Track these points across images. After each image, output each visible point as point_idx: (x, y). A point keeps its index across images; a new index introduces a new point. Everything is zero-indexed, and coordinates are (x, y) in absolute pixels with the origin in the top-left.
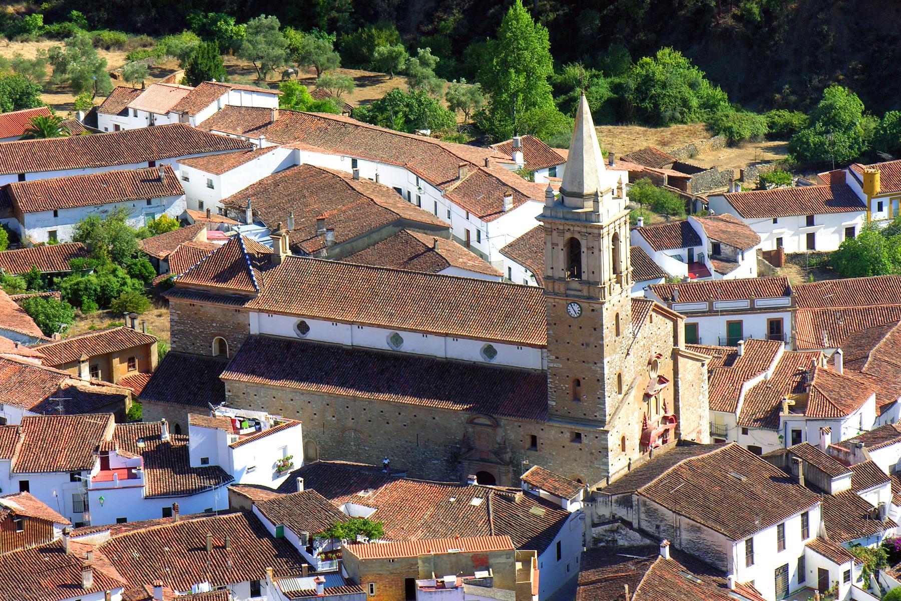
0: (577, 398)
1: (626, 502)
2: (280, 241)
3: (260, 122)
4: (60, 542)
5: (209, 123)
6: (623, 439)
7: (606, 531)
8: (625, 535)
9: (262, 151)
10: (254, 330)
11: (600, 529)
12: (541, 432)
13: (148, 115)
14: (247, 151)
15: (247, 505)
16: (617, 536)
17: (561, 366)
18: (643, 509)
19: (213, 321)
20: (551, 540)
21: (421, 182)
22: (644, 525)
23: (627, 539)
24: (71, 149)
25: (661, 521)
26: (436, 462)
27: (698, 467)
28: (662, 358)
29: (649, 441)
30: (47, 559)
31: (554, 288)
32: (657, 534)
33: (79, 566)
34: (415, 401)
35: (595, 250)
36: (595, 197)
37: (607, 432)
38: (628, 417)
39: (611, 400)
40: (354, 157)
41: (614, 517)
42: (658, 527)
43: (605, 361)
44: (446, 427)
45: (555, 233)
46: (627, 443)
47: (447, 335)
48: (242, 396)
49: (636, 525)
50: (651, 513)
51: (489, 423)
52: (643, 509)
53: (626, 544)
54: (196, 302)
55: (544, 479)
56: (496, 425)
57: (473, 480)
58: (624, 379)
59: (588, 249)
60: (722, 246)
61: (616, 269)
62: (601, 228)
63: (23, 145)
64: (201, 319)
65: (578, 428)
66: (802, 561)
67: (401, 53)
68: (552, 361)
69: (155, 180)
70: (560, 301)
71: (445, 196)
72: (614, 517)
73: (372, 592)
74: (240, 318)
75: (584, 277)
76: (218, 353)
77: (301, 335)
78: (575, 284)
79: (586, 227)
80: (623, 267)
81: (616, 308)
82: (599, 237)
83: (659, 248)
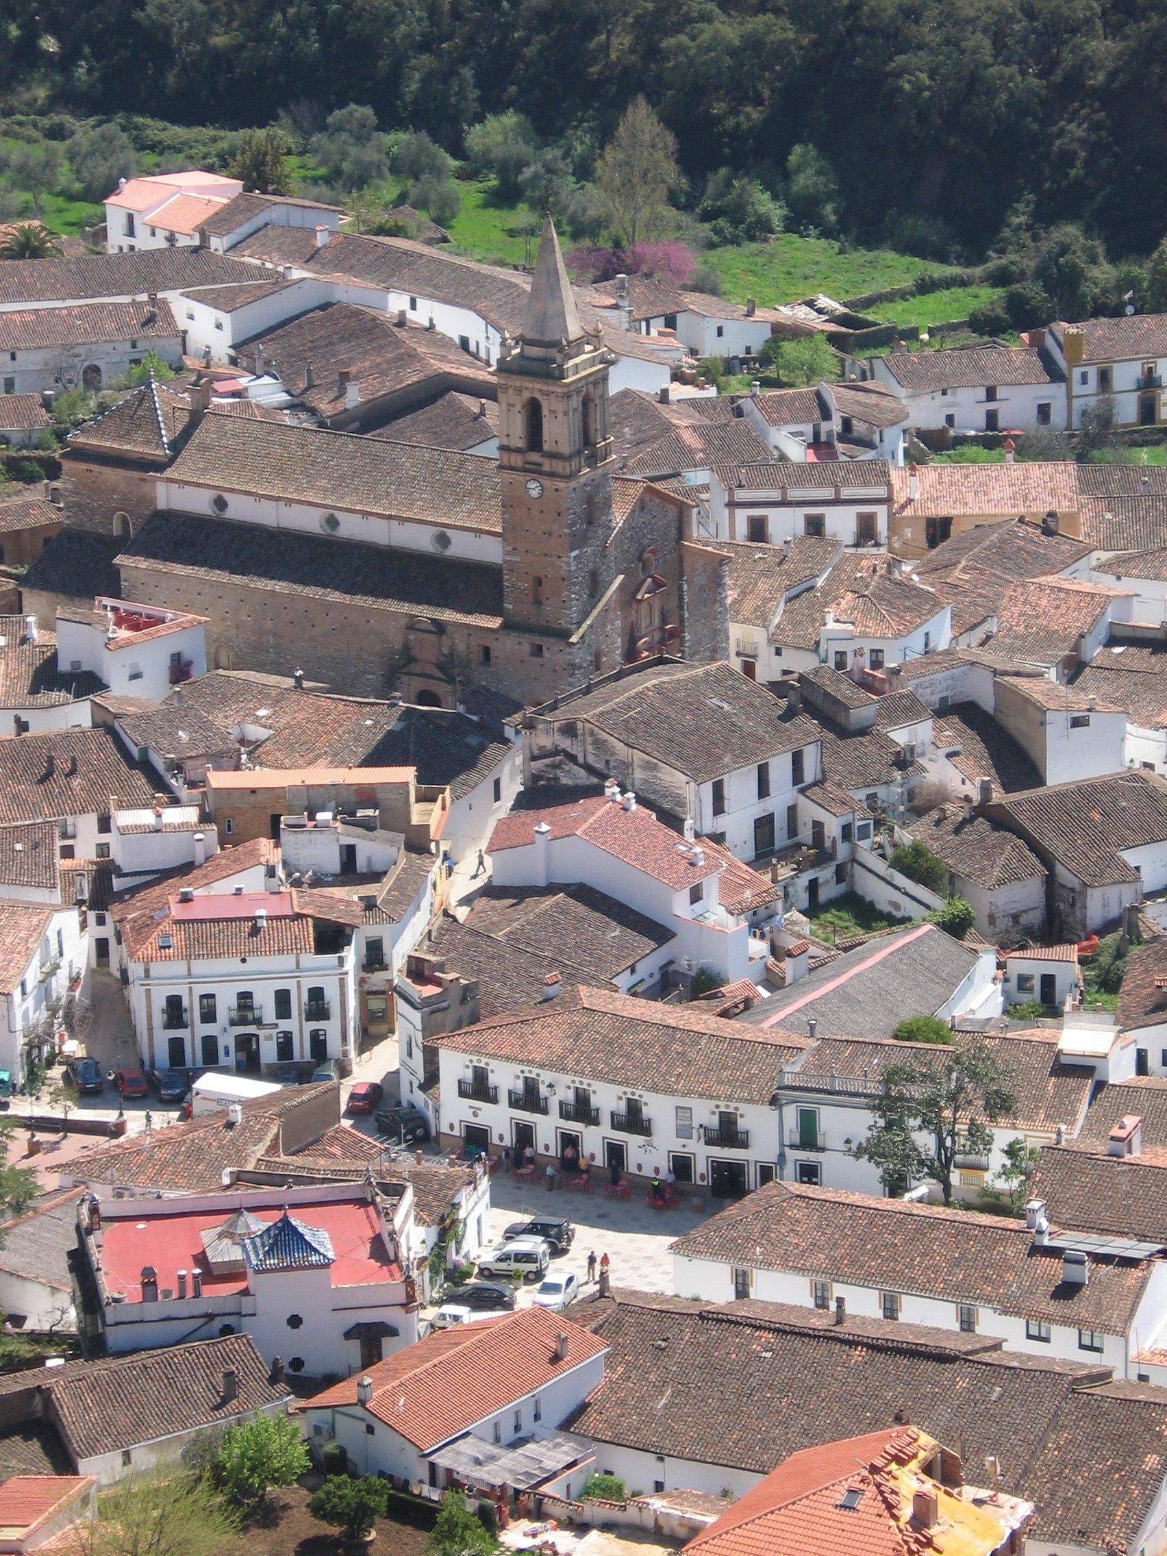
0: (538, 602)
7: (547, 766)
10: (162, 504)
15: (109, 719)
18: (589, 740)
19: (114, 492)
22: (591, 760)
23: (573, 776)
34: (347, 599)
42: (607, 762)
47: (390, 517)
48: (141, 587)
49: (581, 760)
50: (599, 744)
52: (589, 740)
53: (570, 782)
60: (854, 422)
65: (538, 640)
66: (792, 810)
67: (1075, 152)
70: (518, 478)
74: (146, 488)
75: (546, 447)
83: (774, 422)
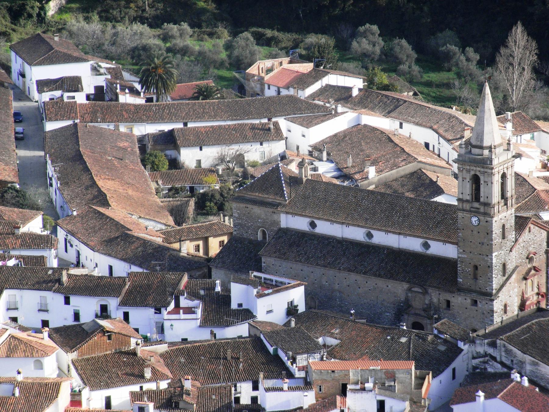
0: (475, 278)
1: (493, 345)
2: (303, 170)
3: (343, 95)
4: (134, 349)
5: (313, 96)
6: (505, 306)
7: (480, 362)
8: (492, 365)
9: (337, 114)
10: (283, 225)
11: (477, 361)
12: (453, 299)
13: (276, 89)
14: (329, 114)
16: (487, 366)
17: (466, 256)
19: (259, 218)
20: (448, 366)
21: (441, 139)
22: (504, 360)
23: (494, 368)
24: (219, 108)
25: (514, 357)
26: (388, 314)
27: (544, 325)
28: (537, 256)
29: (524, 308)
30: (125, 359)
31: (463, 206)
32: (511, 366)
33: (142, 363)
35: (489, 183)
36: (490, 148)
37: (493, 300)
38: (509, 291)
39: (497, 280)
40: (401, 121)
41: (486, 353)
42: (512, 361)
43: (494, 254)
44: (395, 292)
45: (464, 171)
46: (508, 308)
48: (272, 266)
49: (498, 359)
51: (420, 291)
54: (250, 206)
55: (449, 328)
56: (425, 293)
57: (403, 326)
58: (508, 267)
59: (485, 182)
61: (503, 196)
62: (492, 169)
63: (188, 104)
64: (252, 216)
68: (461, 253)
69: (266, 130)
70: (467, 215)
71: (453, 149)
72: (486, 353)
73: (320, 391)
75: (482, 200)
76: (262, 239)
77: (312, 230)
78: (476, 205)
79: (483, 167)
80: (509, 195)
81: (503, 221)
82: (492, 174)
